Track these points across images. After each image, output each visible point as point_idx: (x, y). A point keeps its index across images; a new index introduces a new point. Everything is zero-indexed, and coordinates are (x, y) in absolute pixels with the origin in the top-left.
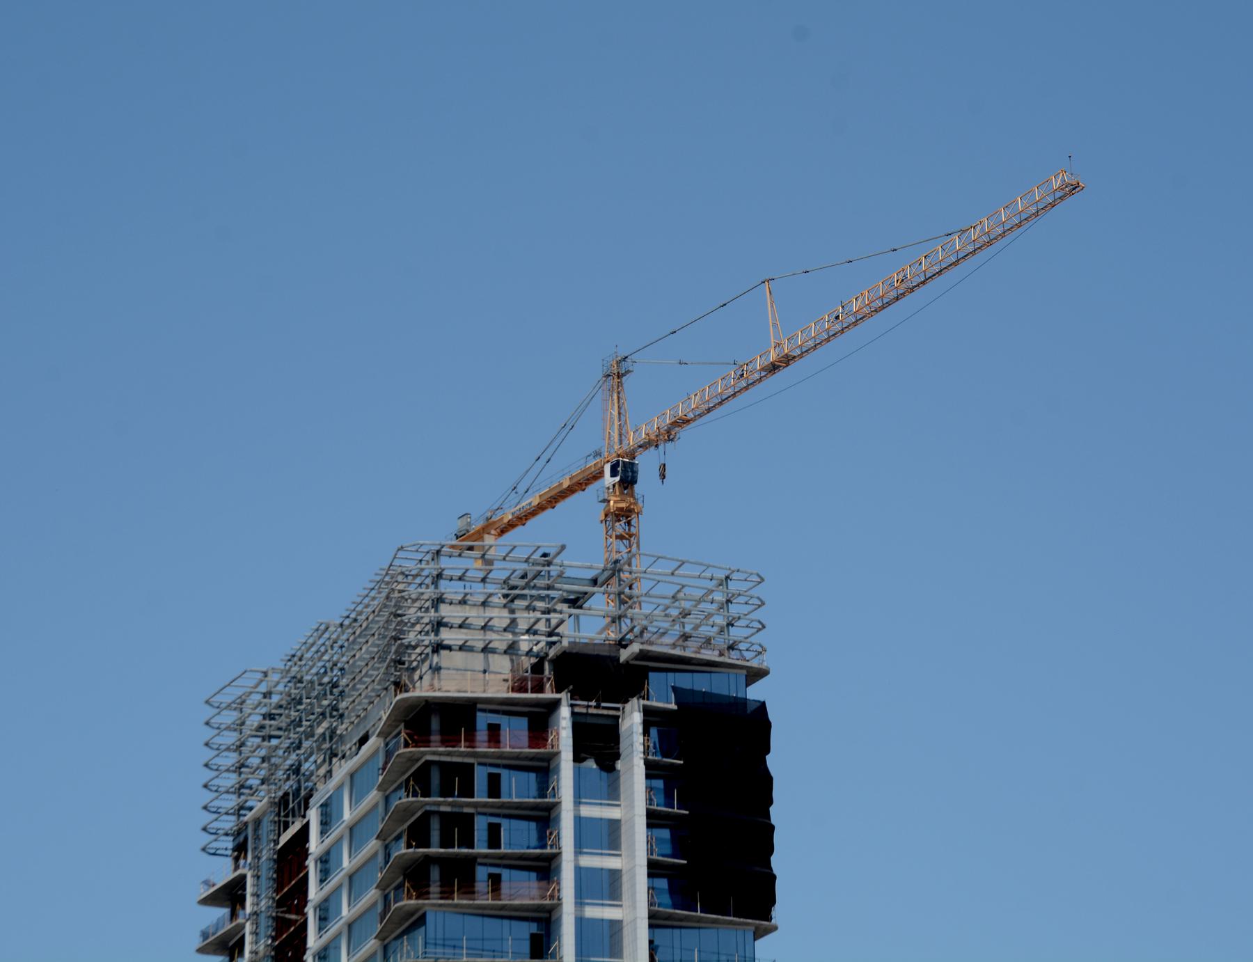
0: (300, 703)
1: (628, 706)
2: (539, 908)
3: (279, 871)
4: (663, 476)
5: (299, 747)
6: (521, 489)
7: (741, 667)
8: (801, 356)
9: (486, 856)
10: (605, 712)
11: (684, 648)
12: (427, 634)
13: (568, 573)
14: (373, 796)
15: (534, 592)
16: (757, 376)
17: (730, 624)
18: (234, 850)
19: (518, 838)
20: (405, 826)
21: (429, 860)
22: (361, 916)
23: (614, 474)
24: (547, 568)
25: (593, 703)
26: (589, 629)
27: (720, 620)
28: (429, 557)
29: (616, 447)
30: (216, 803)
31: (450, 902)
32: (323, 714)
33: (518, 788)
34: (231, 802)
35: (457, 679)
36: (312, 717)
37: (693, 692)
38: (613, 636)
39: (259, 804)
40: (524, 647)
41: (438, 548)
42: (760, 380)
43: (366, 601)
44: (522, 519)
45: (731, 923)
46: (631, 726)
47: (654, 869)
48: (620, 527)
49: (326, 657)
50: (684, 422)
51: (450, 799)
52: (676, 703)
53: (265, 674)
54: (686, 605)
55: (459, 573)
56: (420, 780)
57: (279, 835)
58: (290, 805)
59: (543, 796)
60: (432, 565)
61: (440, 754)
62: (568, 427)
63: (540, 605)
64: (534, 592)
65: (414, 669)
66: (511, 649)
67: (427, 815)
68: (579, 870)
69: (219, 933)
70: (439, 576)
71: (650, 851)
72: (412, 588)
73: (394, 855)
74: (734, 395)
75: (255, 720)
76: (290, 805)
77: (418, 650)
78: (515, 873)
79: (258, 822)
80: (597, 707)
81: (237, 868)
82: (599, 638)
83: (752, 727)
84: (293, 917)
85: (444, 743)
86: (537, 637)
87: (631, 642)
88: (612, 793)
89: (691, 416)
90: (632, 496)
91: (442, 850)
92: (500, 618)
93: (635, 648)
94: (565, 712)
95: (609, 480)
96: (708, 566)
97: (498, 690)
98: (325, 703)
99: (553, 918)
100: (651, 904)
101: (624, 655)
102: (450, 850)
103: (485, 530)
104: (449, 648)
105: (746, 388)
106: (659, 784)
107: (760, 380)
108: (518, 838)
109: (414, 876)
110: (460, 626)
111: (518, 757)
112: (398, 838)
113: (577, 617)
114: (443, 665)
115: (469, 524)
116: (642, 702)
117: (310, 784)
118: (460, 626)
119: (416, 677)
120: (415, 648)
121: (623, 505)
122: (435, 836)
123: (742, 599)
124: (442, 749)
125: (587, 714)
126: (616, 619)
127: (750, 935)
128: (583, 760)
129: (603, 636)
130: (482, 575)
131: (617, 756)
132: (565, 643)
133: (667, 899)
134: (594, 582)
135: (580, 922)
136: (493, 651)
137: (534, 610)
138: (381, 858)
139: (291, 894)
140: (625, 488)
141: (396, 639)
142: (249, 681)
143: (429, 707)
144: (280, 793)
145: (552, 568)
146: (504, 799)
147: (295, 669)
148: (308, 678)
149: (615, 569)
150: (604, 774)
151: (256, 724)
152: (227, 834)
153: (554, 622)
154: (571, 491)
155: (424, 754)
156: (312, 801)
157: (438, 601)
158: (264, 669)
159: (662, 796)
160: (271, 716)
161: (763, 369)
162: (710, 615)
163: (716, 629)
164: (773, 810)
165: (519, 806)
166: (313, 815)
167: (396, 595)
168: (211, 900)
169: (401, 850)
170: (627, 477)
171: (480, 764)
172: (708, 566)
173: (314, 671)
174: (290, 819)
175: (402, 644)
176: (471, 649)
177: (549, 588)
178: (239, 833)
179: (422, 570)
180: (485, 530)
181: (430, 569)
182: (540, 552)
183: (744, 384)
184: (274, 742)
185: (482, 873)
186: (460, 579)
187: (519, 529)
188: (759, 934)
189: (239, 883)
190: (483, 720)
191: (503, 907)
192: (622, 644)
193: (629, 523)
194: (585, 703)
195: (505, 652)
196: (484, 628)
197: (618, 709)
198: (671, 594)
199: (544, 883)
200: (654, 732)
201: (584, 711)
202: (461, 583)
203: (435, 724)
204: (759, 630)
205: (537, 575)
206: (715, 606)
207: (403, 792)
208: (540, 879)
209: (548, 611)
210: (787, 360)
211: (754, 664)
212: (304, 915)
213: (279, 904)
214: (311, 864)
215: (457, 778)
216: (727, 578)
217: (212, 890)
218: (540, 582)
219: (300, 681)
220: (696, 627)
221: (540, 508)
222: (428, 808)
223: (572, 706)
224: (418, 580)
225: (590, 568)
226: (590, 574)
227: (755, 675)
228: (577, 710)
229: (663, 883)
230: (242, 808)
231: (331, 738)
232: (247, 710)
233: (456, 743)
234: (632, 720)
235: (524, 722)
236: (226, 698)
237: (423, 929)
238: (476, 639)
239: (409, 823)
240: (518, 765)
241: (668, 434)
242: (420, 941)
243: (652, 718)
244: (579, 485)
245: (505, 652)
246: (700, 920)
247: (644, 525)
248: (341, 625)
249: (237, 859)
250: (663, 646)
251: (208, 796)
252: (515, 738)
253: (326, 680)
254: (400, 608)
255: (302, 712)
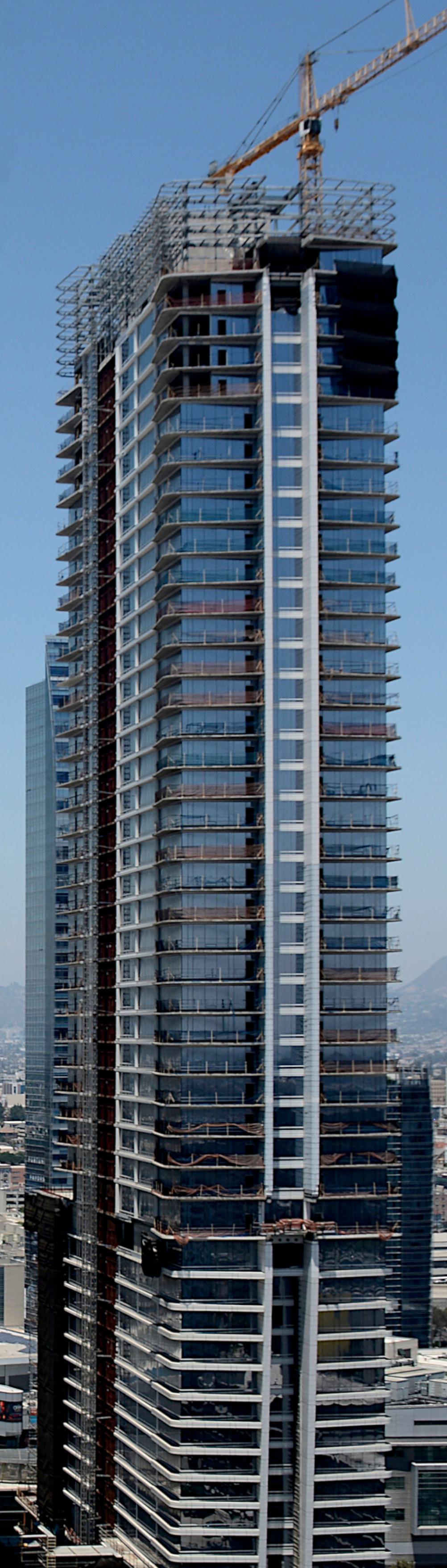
0: (109, 284)
1: (306, 274)
2: (250, 399)
3: (99, 384)
4: (337, 127)
5: (109, 311)
6: (248, 142)
7: (380, 245)
8: (427, 40)
9: (217, 370)
10: (292, 279)
11: (344, 236)
12: (181, 237)
13: (268, 194)
14: (150, 338)
15: (246, 207)
16: (397, 56)
17: (372, 219)
18: (76, 373)
19: (236, 359)
20: (168, 355)
21: (181, 373)
22: (145, 409)
23: (306, 127)
24: (255, 191)
25: (284, 274)
26: (281, 228)
27: (366, 217)
28: (180, 190)
29: (308, 110)
30: (64, 347)
31: (194, 398)
32: (122, 290)
33: (236, 329)
34: (73, 345)
35: (196, 265)
36: (116, 293)
37: (347, 263)
38: (297, 230)
39: (87, 346)
40: (242, 240)
41: (185, 184)
42: (400, 59)
43: (145, 220)
44: (248, 162)
45: (369, 402)
46: (307, 287)
47: (321, 372)
48: (309, 162)
49: (123, 256)
50: (351, 90)
51: (195, 337)
52: (337, 270)
53: (90, 268)
54: (346, 208)
55: (199, 199)
56: (177, 327)
57: (99, 363)
58: (103, 347)
59: (252, 331)
60: (183, 195)
61: (189, 310)
62: (277, 100)
63: (251, 215)
64: (246, 207)
65: (173, 260)
66: (233, 243)
67: (181, 347)
68: (274, 376)
69: (68, 421)
70: (187, 201)
71: (319, 361)
72: (171, 210)
73: (162, 371)
74: (383, 70)
75: (85, 297)
76: (103, 347)
77: (175, 248)
78: (235, 379)
79: (86, 356)
80: (287, 276)
81: (77, 383)
82: (289, 234)
83: (387, 282)
84: (108, 410)
85: (191, 303)
86: (248, 235)
87: (309, 234)
88: (296, 328)
89: (355, 86)
90: (317, 140)
91: (190, 368)
92: (226, 224)
93: (311, 237)
94: (265, 280)
95: (303, 132)
96: (359, 183)
97: (226, 269)
98: (123, 283)
99: (259, 404)
100: (319, 393)
101: (304, 242)
102: (195, 368)
103: (226, 170)
104: (193, 245)
105: (391, 64)
106: (326, 321)
107: (400, 59)
108: (236, 359)
109: (175, 383)
110: (201, 231)
111: (237, 309)
112: (165, 362)
113: (276, 221)
114: (190, 255)
115: (216, 167)
116: (316, 271)
117: (115, 333)
118: (201, 231)
119: (174, 264)
120: (173, 246)
121: (311, 148)
122: (186, 359)
123: (381, 202)
124: (189, 307)
125: (279, 281)
126: (300, 220)
127: (381, 408)
128: (278, 309)
129: (291, 232)
130: (213, 199)
131: (299, 304)
132: (266, 237)
133: (329, 389)
134: (286, 198)
135: (275, 406)
136: (221, 245)
137: (247, 218)
138: (155, 374)
139: (107, 399)
140: (313, 136)
141: (162, 241)
142: (80, 274)
143: (181, 281)
144: (99, 340)
145: (258, 191)
146: (228, 335)
147: (106, 264)
148: (113, 269)
149: (299, 188)
150: (291, 317)
151: (85, 299)
152: (70, 364)
153: (259, 225)
154: (279, 141)
155: (179, 311)
156: (116, 343)
157: (186, 217)
158: (89, 265)
159: (327, 327)
160: (94, 294)
161: (401, 52)
162: (360, 214)
163: (363, 222)
164: (397, 332)
165: (237, 339)
166: (118, 351)
167: (162, 214)
168: (61, 403)
169: (166, 368)
170: (314, 129)
171: (214, 315)
172: (359, 183)
173: (116, 265)
174: (105, 354)
175: (164, 246)
176: (207, 245)
177: (256, 203)
178: (76, 364)
179: (177, 198)
180: (226, 170)
181: (182, 197)
182: (251, 181)
183: (389, 62)
184: (96, 309)
185: (214, 380)
186: (200, 202)
187: (247, 169)
188: (387, 407)
189: (78, 391)
190: (214, 288)
191: (228, 399)
192: (303, 235)
193: (315, 159)
194: (278, 274)
195: (229, 246)
196: (215, 231)
197: (299, 276)
198: (335, 202)
199: (252, 384)
200: (323, 289)
201: (278, 278)
202: (202, 205)
203: (185, 292)
204: (391, 221)
205: (249, 196)
206: (363, 208)
207: (167, 335)
208: (250, 381)
209: (255, 218)
210: (417, 44)
211: (388, 242)
212: (114, 409)
213: (100, 403)
214: (117, 379)
215: (200, 324)
216: (371, 189)
217: (63, 397)
218: (250, 200)
219: (109, 271)
220: (352, 222)
221: (260, 154)
222: (181, 343)
223: (270, 276)
224: (175, 205)
225: (283, 189)
226: (284, 193)
227: (389, 249)
228: (273, 278)
229: (327, 380)
230: (79, 348)
231: (127, 304)
232: (80, 291)
233: (199, 303)
234: (309, 282)
235: (240, 288)
236: (67, 284)
237: (179, 415)
238: (211, 239)
239: (171, 352)
240: (238, 314)
241: (341, 100)
242: (178, 422)
243: (320, 281)
244: (284, 137)
245: (229, 246)
246: (349, 401)
247: (324, 159)
248: (131, 236)
249: (77, 378)
250: (330, 235)
251: (59, 343)
252: (235, 298)
253: (123, 270)
254: (164, 223)
255: (110, 290)
